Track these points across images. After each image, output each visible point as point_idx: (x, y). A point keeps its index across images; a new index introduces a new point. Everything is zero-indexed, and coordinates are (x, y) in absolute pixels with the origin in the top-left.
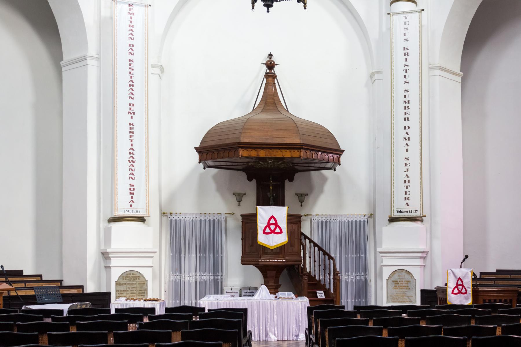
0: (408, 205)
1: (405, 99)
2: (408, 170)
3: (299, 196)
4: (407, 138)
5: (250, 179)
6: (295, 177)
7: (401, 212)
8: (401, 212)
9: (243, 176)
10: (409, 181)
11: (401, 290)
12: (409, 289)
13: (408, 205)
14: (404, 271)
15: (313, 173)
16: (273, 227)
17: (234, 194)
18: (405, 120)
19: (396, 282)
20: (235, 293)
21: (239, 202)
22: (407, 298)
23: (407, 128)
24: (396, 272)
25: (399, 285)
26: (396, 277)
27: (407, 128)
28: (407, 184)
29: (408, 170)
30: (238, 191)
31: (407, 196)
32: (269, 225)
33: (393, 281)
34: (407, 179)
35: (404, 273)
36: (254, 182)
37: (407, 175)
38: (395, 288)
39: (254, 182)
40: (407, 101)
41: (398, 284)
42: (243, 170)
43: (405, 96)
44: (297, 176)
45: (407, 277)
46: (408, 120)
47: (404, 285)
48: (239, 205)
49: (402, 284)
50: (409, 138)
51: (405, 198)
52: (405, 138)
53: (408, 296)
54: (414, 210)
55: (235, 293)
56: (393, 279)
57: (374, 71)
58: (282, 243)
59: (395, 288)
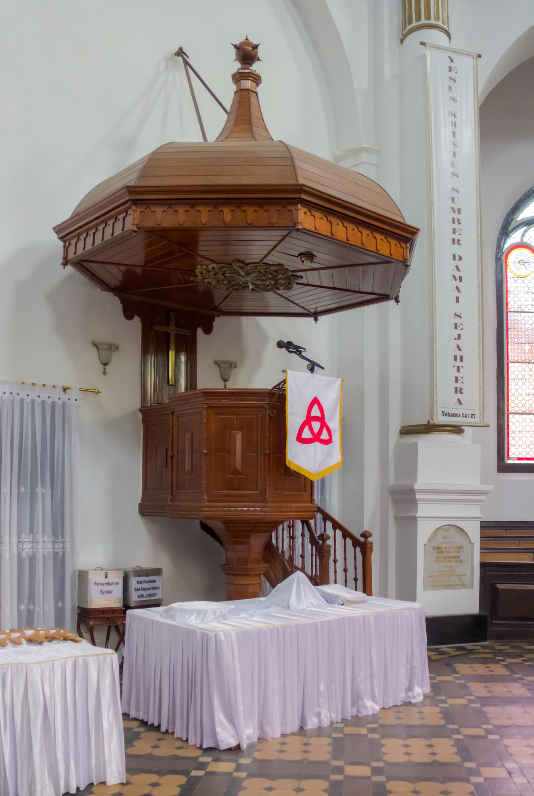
0: (460, 403)
1: (453, 205)
2: (459, 336)
3: (223, 365)
4: (457, 277)
5: (129, 316)
6: (214, 324)
7: (448, 415)
8: (448, 415)
9: (113, 303)
10: (461, 357)
11: (448, 564)
12: (461, 561)
13: (460, 403)
14: (453, 528)
15: (245, 320)
16: (316, 426)
17: (95, 345)
18: (454, 242)
19: (439, 550)
20: (112, 584)
21: (105, 364)
22: (456, 578)
23: (457, 258)
24: (440, 530)
25: (445, 555)
26: (439, 541)
27: (457, 258)
28: (458, 363)
29: (459, 336)
30: (104, 338)
31: (458, 385)
32: (309, 420)
33: (434, 548)
34: (458, 354)
35: (453, 533)
36: (137, 322)
37: (458, 346)
38: (438, 560)
39: (137, 322)
40: (456, 209)
41: (442, 552)
42: (115, 290)
43: (453, 199)
44: (219, 322)
45: (459, 539)
46: (459, 244)
47: (453, 554)
48: (105, 373)
49: (449, 552)
50: (460, 278)
51: (456, 389)
52: (454, 276)
53: (459, 576)
54: (469, 412)
55: (112, 584)
56: (435, 544)
57: (364, 145)
58: (301, 469)
59: (438, 560)
